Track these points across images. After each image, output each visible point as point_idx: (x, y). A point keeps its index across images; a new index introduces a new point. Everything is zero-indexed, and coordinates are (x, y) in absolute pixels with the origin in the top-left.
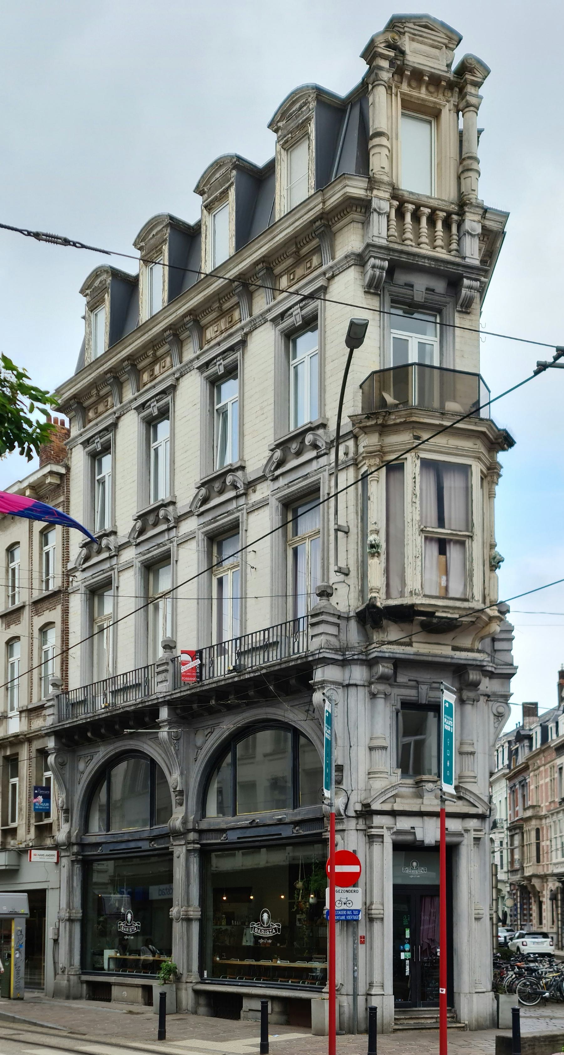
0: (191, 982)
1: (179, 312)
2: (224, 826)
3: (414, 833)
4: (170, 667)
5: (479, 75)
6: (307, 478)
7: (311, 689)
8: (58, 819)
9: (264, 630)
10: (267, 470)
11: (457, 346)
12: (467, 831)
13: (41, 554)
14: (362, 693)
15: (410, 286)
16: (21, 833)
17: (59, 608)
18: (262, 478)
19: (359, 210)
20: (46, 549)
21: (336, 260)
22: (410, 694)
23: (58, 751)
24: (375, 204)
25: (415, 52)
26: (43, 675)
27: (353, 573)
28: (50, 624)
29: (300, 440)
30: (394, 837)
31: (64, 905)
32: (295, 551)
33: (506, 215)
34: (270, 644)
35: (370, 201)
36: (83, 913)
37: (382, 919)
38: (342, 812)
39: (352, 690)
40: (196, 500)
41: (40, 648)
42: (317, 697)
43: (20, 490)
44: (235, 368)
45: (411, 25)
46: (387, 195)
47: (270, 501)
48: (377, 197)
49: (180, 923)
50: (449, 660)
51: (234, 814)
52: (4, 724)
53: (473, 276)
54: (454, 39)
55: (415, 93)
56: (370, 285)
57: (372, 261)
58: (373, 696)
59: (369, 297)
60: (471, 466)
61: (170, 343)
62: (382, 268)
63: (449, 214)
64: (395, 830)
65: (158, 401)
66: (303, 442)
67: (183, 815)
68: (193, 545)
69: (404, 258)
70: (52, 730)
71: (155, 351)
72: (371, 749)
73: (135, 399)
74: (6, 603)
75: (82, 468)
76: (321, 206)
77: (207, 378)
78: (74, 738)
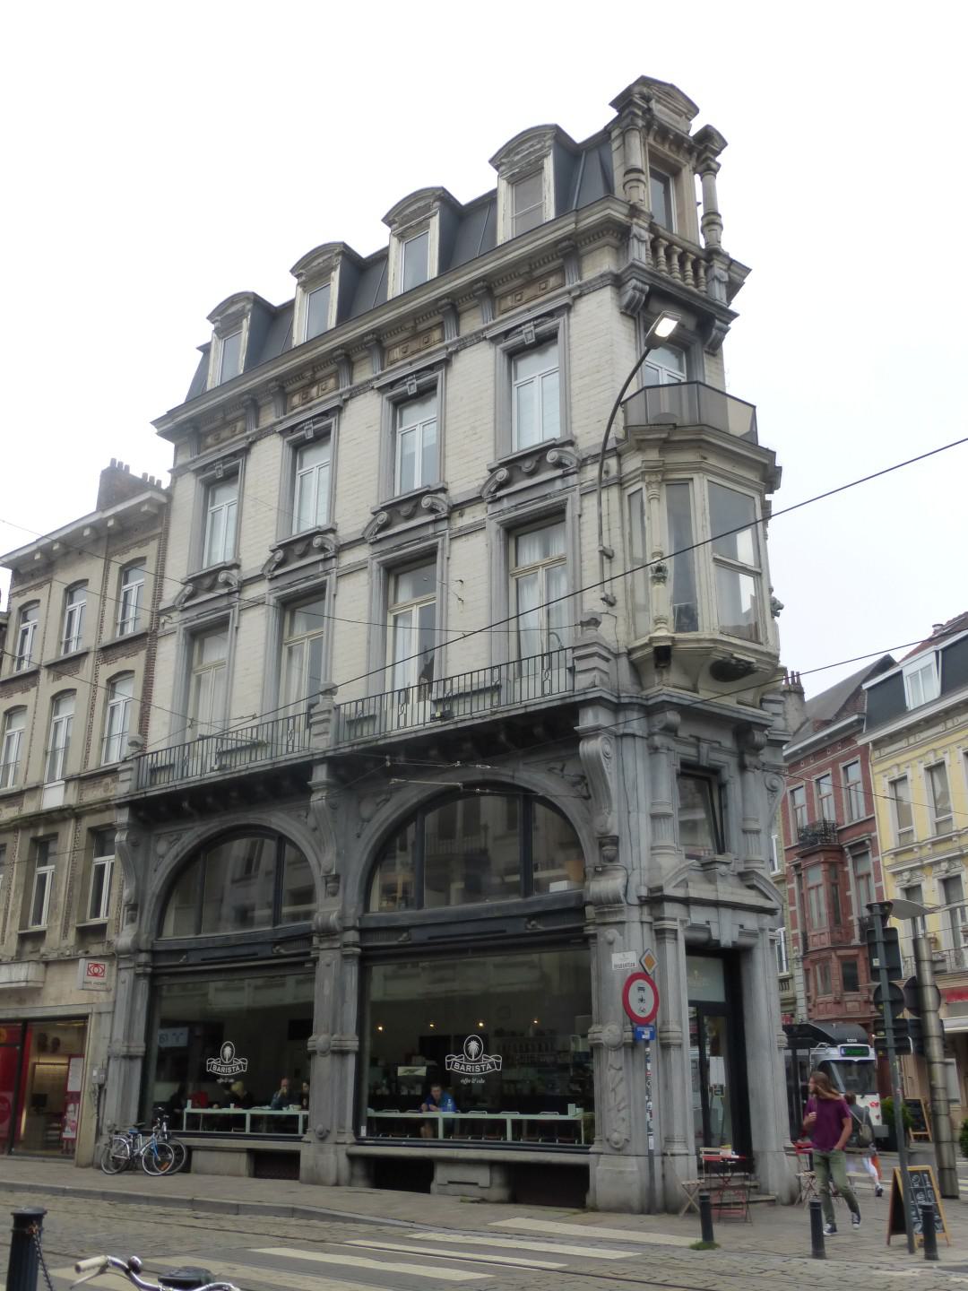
0: (344, 1143)
1: (358, 330)
2: (406, 923)
4: (333, 717)
6: (547, 499)
7: (577, 738)
8: (118, 919)
9: (357, 701)
10: (485, 491)
13: (17, 632)
14: (640, 745)
16: (54, 938)
17: (143, 654)
18: (258, 578)
20: (70, 607)
21: (583, 281)
22: (690, 752)
23: (130, 827)
24: (635, 230)
26: (106, 735)
27: (620, 604)
28: (127, 673)
29: (213, 577)
31: (119, 1033)
32: (290, 650)
33: (748, 270)
34: (366, 718)
36: (147, 1047)
38: (622, 897)
39: (628, 742)
40: (373, 525)
41: (106, 703)
42: (588, 747)
43: (100, 519)
44: (328, 433)
46: (646, 225)
47: (368, 565)
48: (637, 224)
49: (329, 1057)
50: (735, 715)
51: (420, 906)
52: (38, 798)
54: (693, 110)
55: (660, 147)
56: (627, 307)
57: (634, 282)
58: (654, 750)
59: (624, 318)
61: (339, 363)
62: (642, 291)
64: (689, 924)
65: (314, 423)
66: (216, 579)
67: (339, 907)
68: (362, 578)
70: (128, 799)
71: (315, 373)
73: (281, 422)
74: (58, 650)
75: (192, 496)
76: (573, 226)
77: (290, 443)
78: (154, 812)
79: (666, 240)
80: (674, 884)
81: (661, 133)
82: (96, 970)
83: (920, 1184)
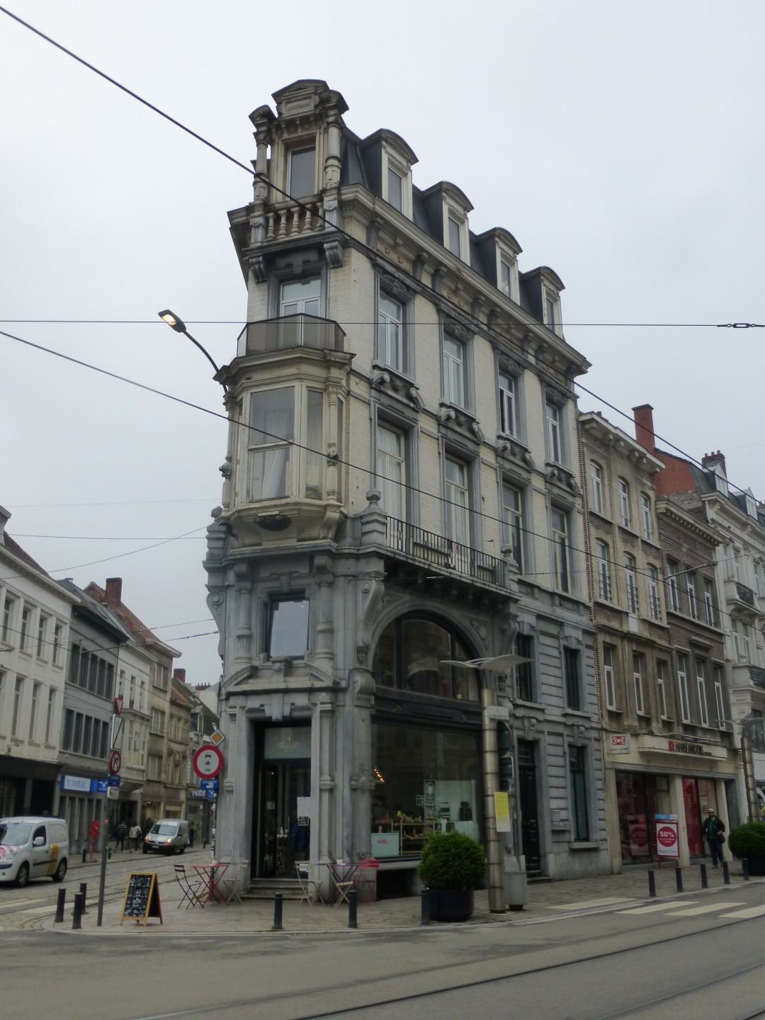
3: (264, 711)
15: (290, 265)
19: (348, 209)
30: (248, 715)
50: (293, 551)
53: (332, 239)
59: (260, 285)
62: (258, 263)
64: (246, 709)
79: (282, 209)
80: (235, 683)
81: (299, 118)
82: (619, 740)
83: (142, 884)
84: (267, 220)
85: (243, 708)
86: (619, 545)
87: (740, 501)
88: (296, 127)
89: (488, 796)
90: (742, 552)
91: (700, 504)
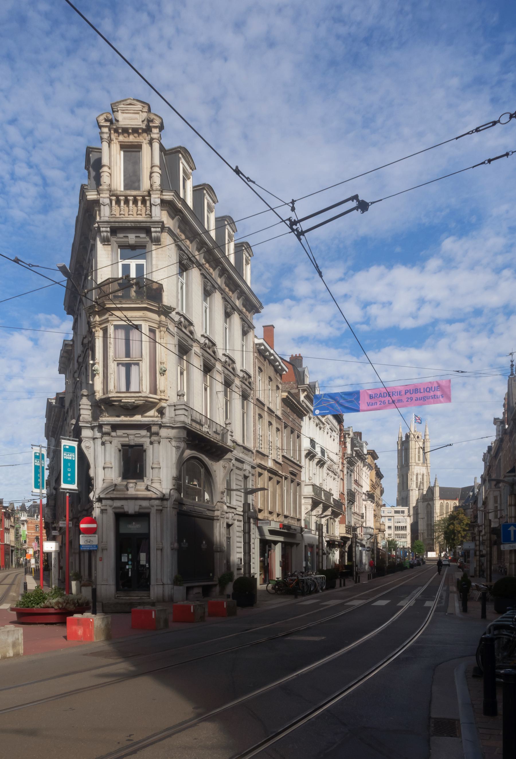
3: (123, 508)
5: (157, 122)
11: (154, 262)
12: (153, 506)
25: (125, 119)
30: (114, 510)
35: (99, 200)
37: (107, 549)
45: (122, 106)
48: (102, 197)
50: (139, 423)
55: (126, 140)
60: (141, 325)
62: (107, 232)
63: (143, 197)
69: (117, 225)
72: (104, 468)
84: (111, 201)
85: (111, 506)
86: (266, 415)
87: (312, 387)
88: (129, 134)
89: (514, 517)
90: (312, 419)
91: (297, 391)
